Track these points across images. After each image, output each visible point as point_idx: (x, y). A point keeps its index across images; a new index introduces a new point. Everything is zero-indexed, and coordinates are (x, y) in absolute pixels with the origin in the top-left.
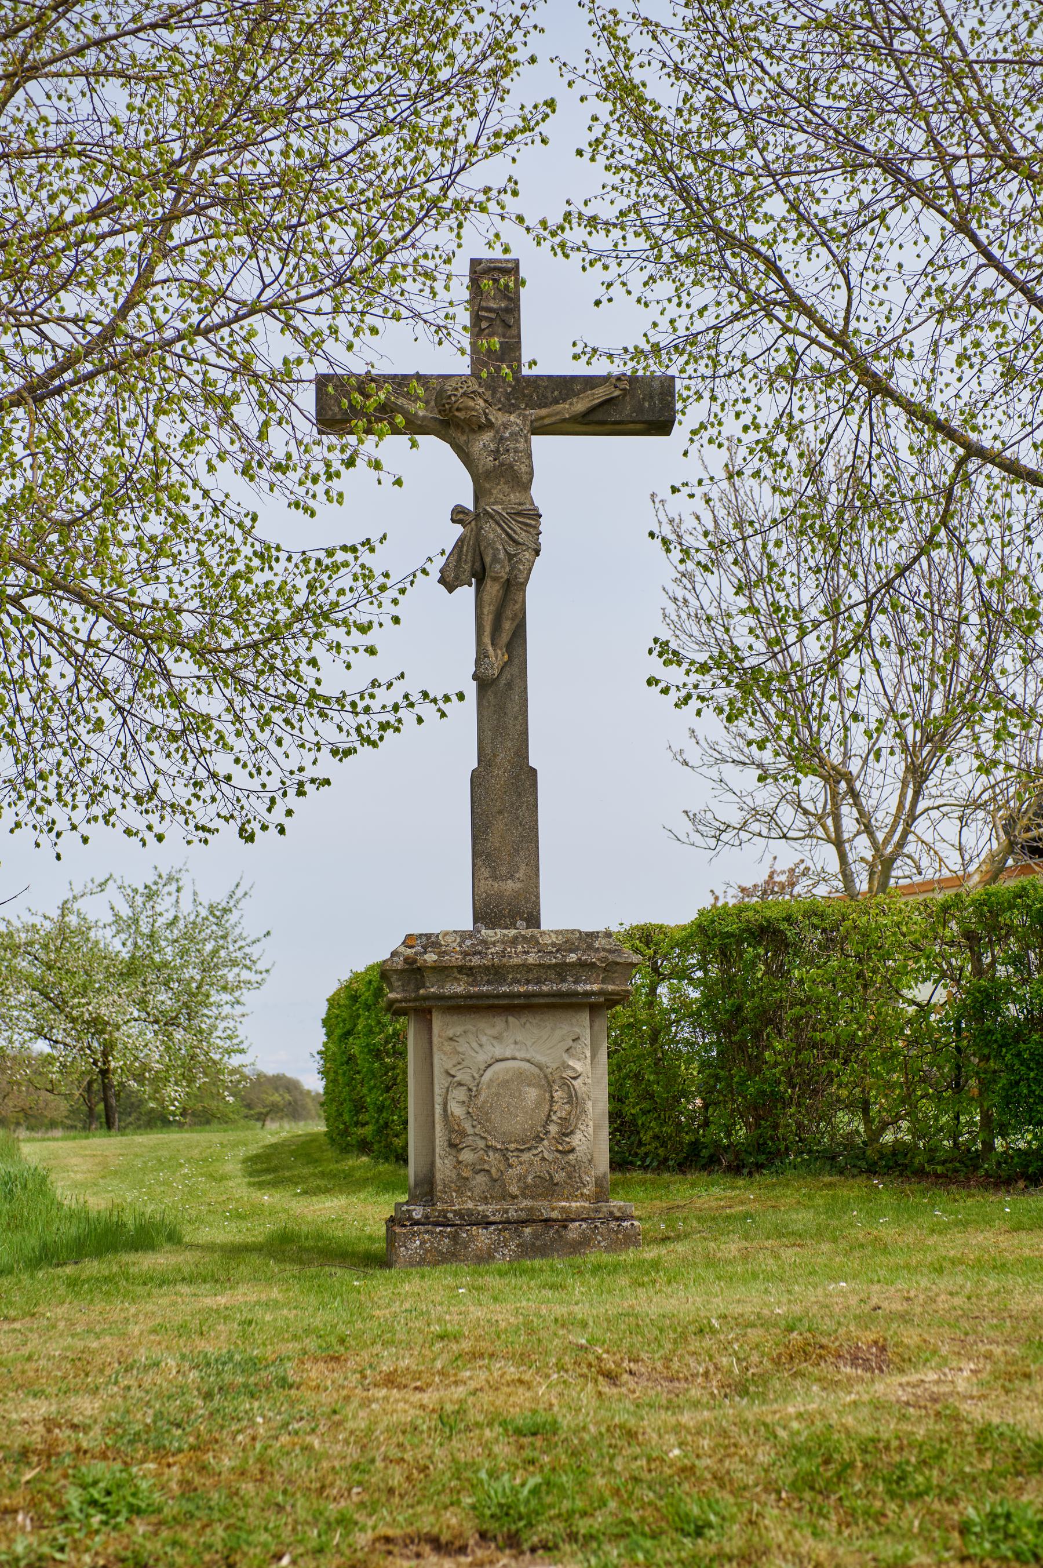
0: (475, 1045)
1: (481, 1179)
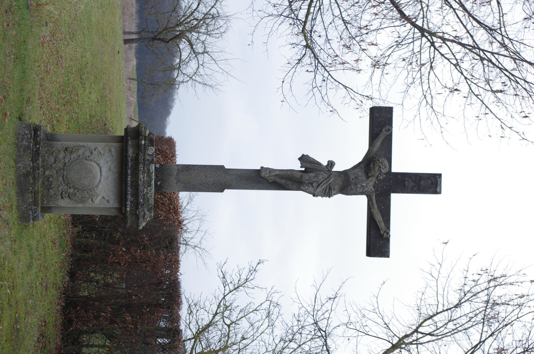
0: (107, 159)
1: (52, 160)
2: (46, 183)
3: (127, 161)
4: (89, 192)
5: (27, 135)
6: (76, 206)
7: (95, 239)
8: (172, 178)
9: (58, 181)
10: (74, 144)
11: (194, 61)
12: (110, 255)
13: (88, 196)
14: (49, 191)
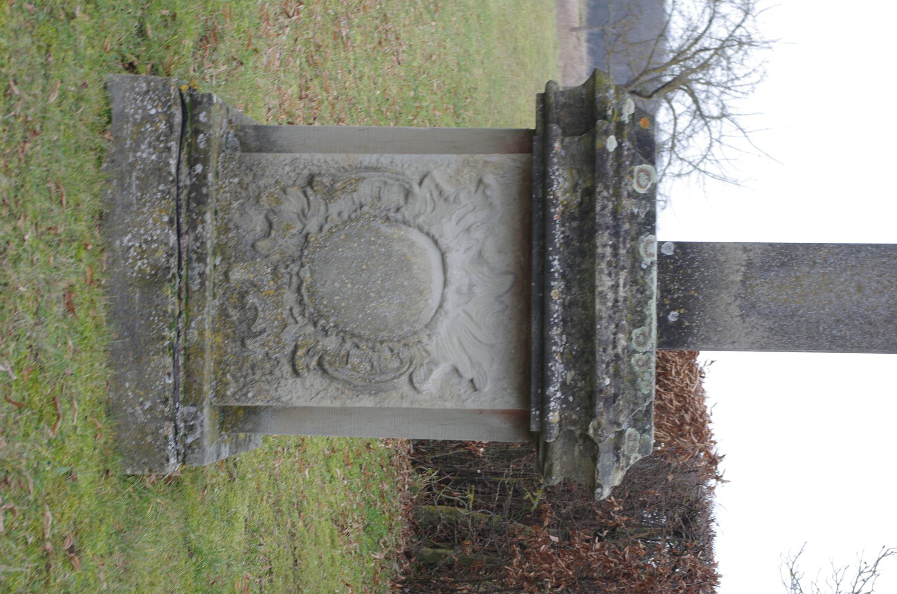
0: (470, 219)
1: (258, 223)
2: (235, 315)
3: (546, 221)
4: (398, 347)
5: (153, 123)
6: (349, 404)
7: (475, 508)
8: (725, 296)
9: (278, 305)
10: (341, 159)
11: (701, 133)
12: (514, 556)
13: (395, 364)
14: (243, 345)
